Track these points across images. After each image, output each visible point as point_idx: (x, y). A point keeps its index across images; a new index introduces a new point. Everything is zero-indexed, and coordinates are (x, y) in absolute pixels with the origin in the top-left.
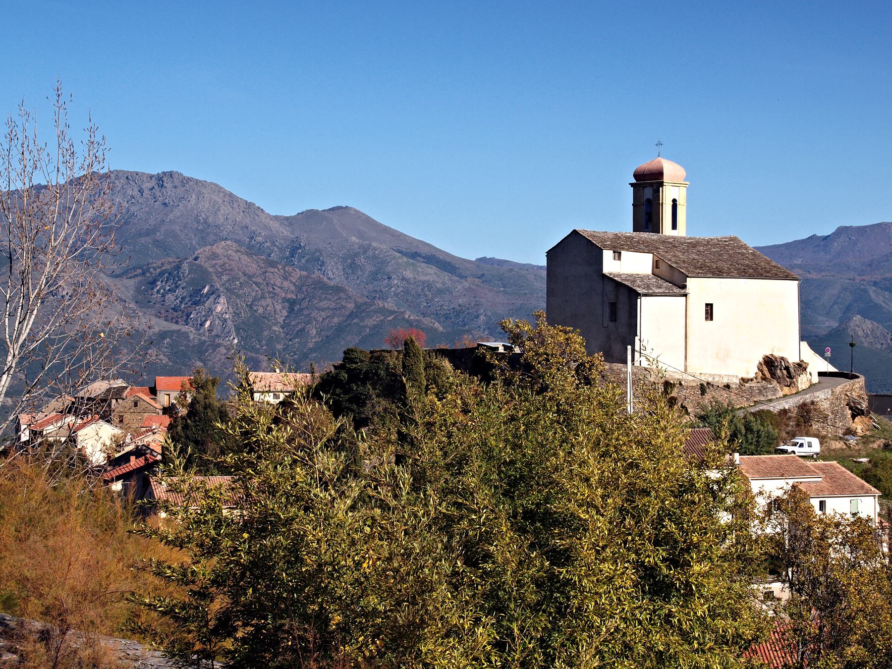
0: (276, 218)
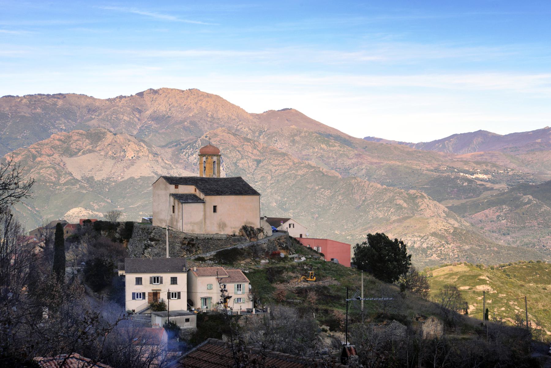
0: (252, 115)
